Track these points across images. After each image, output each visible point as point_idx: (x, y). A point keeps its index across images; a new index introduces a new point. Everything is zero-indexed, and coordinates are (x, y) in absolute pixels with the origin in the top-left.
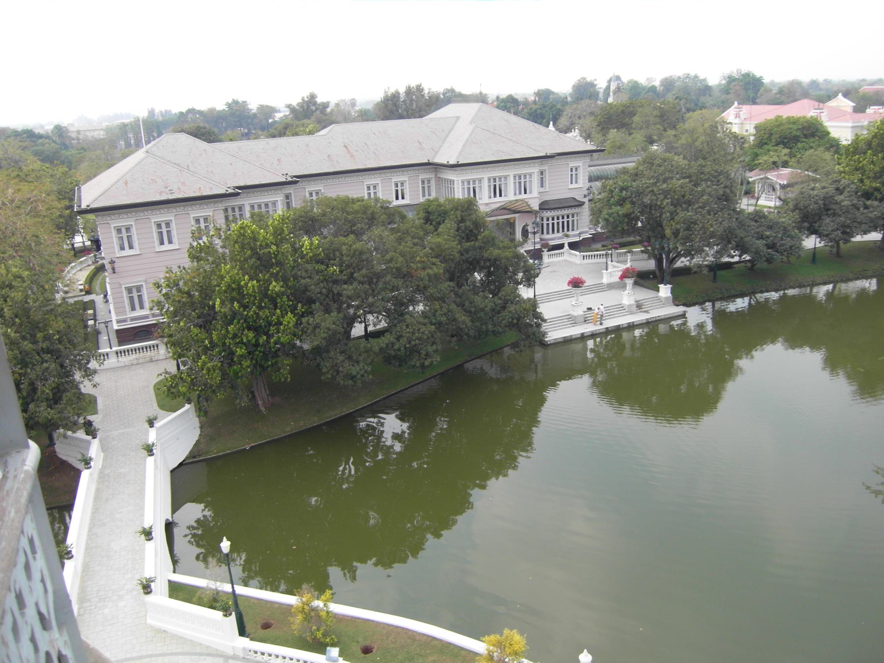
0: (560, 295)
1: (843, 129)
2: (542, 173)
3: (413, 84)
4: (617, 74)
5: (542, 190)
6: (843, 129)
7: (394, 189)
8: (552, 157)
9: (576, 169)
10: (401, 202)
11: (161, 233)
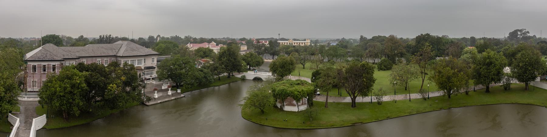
1: (216, 49)
6: (216, 49)
8: (148, 55)
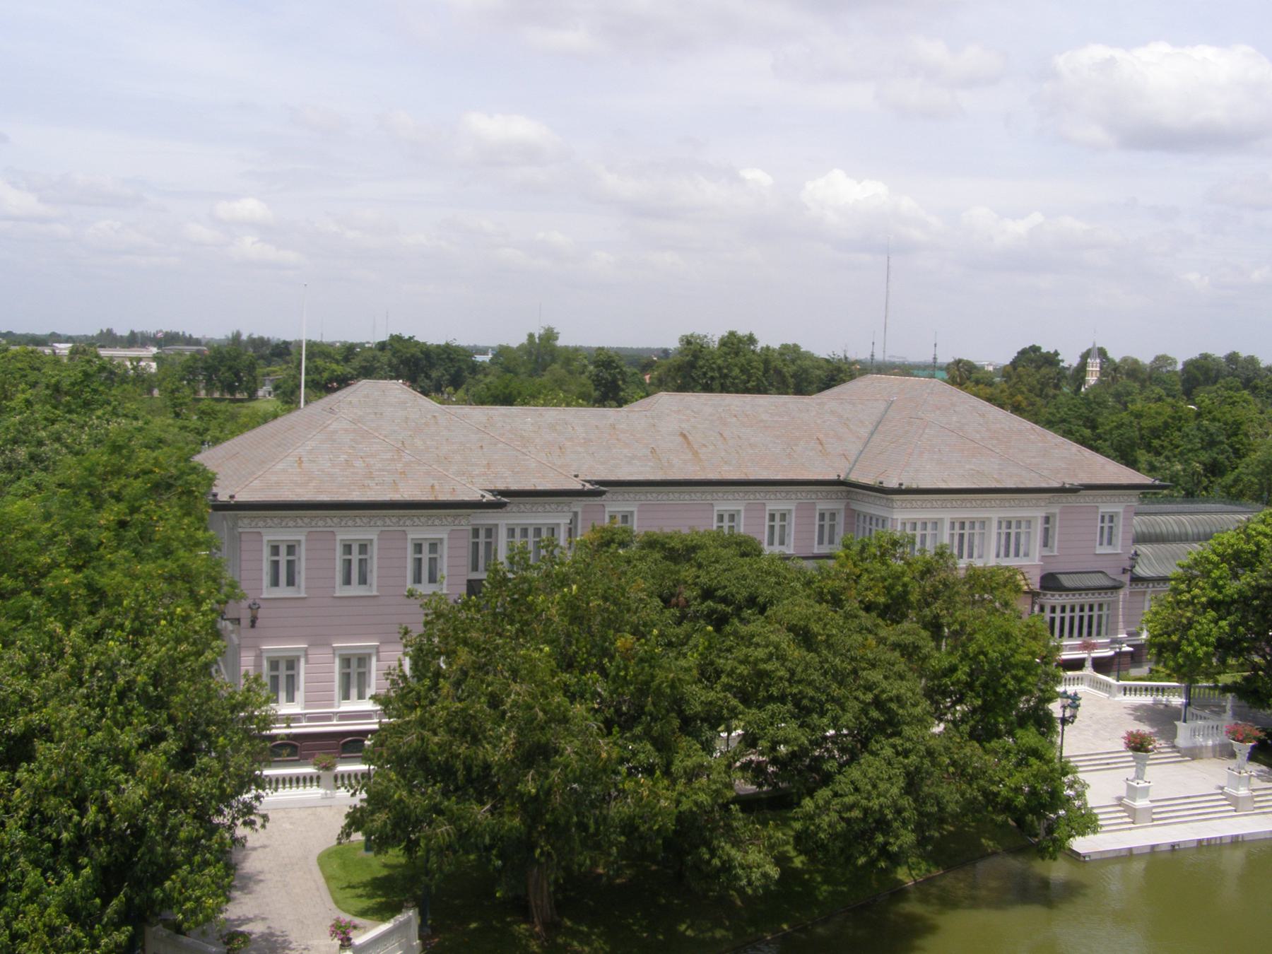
0: (1106, 763)
2: (1047, 520)
3: (742, 331)
7: (767, 523)
8: (1073, 490)
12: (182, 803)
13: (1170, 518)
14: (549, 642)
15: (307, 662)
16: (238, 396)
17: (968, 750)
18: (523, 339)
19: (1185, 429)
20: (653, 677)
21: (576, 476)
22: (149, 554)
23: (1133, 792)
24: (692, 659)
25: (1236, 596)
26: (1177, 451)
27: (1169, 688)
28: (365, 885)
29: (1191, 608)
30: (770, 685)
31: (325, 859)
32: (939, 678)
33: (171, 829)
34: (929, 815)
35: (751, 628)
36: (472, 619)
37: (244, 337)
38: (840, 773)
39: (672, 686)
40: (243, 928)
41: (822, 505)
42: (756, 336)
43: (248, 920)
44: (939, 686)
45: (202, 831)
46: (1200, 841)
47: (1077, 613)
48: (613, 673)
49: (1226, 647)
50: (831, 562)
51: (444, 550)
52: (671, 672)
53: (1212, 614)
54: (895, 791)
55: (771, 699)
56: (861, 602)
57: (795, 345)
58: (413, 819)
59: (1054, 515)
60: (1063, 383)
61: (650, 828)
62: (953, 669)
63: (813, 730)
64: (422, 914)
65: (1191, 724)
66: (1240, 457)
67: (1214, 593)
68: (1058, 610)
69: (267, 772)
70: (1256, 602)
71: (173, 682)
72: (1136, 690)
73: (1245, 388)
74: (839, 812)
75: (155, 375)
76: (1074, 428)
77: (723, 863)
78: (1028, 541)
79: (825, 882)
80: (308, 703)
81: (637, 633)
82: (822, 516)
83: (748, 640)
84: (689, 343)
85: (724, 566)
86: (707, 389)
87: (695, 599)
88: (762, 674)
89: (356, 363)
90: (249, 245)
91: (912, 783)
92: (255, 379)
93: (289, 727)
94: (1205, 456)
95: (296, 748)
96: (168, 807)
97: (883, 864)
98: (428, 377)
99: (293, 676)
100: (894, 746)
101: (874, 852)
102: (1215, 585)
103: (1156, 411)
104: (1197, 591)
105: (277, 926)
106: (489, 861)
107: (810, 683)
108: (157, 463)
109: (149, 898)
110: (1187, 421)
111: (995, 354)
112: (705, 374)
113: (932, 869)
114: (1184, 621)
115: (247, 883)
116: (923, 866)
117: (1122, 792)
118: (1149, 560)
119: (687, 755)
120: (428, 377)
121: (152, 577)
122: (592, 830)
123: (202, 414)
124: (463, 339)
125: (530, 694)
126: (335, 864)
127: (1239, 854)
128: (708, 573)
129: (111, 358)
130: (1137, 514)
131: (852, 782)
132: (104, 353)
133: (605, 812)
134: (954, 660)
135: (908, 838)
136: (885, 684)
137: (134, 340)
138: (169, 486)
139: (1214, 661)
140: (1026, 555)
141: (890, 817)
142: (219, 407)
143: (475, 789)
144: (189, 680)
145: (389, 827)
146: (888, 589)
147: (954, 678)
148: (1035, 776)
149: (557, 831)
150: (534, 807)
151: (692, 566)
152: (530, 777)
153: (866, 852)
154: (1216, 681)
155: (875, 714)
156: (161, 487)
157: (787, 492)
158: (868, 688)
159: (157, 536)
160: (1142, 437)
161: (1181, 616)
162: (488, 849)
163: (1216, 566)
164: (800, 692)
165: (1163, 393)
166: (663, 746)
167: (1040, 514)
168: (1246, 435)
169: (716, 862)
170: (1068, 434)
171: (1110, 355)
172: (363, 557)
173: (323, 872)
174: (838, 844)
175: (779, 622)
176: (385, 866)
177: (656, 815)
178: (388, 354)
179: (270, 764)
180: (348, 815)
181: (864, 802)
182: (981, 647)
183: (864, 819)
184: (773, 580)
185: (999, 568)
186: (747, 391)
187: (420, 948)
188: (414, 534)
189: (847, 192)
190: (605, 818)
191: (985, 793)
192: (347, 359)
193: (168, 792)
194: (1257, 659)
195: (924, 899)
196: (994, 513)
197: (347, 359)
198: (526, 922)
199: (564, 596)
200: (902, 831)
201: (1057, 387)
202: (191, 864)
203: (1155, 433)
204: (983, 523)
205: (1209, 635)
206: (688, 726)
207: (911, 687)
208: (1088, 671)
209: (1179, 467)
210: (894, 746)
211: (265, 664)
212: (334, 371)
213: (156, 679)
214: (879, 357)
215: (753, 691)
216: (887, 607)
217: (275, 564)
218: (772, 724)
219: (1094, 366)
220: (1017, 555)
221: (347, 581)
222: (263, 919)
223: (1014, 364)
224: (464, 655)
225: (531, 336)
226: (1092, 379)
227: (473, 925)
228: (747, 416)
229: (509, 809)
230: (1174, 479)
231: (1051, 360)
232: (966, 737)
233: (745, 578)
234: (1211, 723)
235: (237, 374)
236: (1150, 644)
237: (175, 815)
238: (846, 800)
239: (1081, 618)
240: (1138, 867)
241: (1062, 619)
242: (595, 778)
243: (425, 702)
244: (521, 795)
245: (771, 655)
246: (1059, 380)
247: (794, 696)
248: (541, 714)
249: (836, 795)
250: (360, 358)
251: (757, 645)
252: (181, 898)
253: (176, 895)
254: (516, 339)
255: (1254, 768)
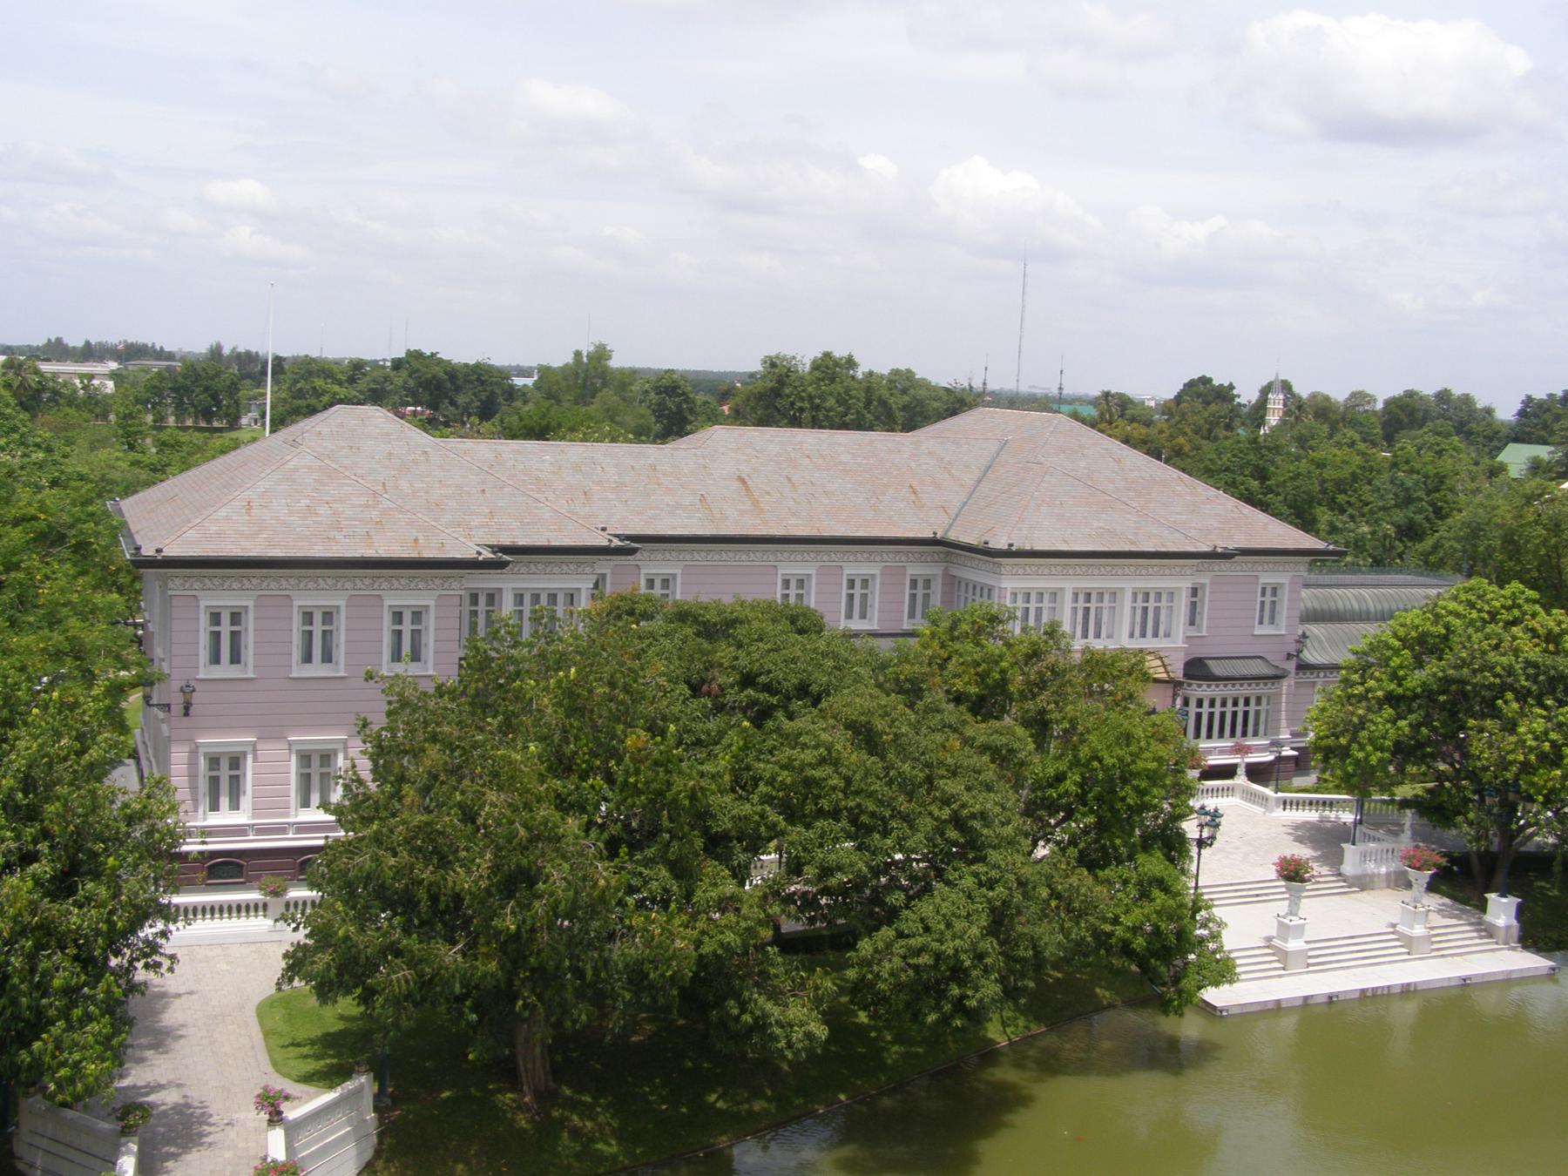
0: (1251, 894)
2: (1194, 592)
3: (840, 352)
4: (1282, 377)
5: (1192, 632)
7: (845, 591)
8: (1227, 555)
9: (1274, 591)
10: (857, 625)
11: (216, 636)
12: (59, 941)
13: (1349, 592)
14: (541, 739)
15: (255, 759)
16: (216, 424)
17: (1074, 880)
18: (569, 359)
19: (1376, 482)
20: (669, 784)
21: (604, 529)
22: (30, 624)
23: (1285, 930)
24: (723, 762)
25: (1419, 690)
26: (1366, 509)
27: (1338, 801)
28: (313, 1043)
29: (1364, 704)
30: (819, 797)
31: (264, 1010)
32: (1041, 788)
33: (43, 975)
34: (1023, 960)
35: (798, 724)
36: (446, 709)
37: (226, 351)
38: (907, 907)
39: (693, 797)
40: (152, 1098)
41: (914, 570)
42: (857, 359)
43: (159, 1087)
44: (1043, 799)
45: (83, 978)
46: (1363, 991)
47: (1229, 708)
48: (621, 779)
49: (1405, 752)
50: (913, 641)
51: (431, 621)
52: (691, 778)
53: (1388, 711)
54: (974, 931)
55: (821, 813)
56: (948, 692)
57: (909, 371)
58: (363, 960)
59: (1203, 586)
60: (1237, 422)
61: (662, 975)
62: (1060, 778)
63: (874, 853)
64: (379, 1078)
65: (1360, 847)
66: (1443, 518)
67: (1393, 686)
68: (1206, 704)
69: (177, 899)
70: (1442, 698)
71: (49, 787)
72: (1298, 804)
73: (1458, 433)
74: (904, 958)
75: (112, 396)
76: (1239, 478)
77: (756, 1019)
78: (1170, 616)
79: (895, 1041)
80: (256, 810)
81: (654, 729)
82: (914, 583)
83: (793, 740)
84: (773, 365)
85: (769, 646)
86: (795, 422)
87: (732, 686)
88: (809, 783)
89: (363, 384)
90: (244, 237)
91: (1000, 921)
92: (237, 403)
93: (204, 843)
94: (1399, 516)
95: (226, 868)
96: (39, 947)
97: (959, 1023)
98: (453, 403)
99: (237, 777)
100: (976, 875)
101: (947, 1007)
102: (1394, 676)
103: (1339, 456)
104: (1372, 683)
105: (195, 1094)
106: (462, 1014)
107: (871, 795)
108: (43, 508)
109: (12, 1063)
110: (1379, 472)
111: (1154, 385)
112: (792, 404)
113: (1032, 1026)
114: (1355, 720)
115: (162, 1039)
116: (1021, 1022)
117: (1272, 931)
118: (1320, 642)
119: (715, 882)
120: (453, 403)
121: (31, 653)
122: (589, 974)
123: (162, 446)
124: (499, 355)
125: (510, 805)
126: (277, 1019)
127: (1411, 1007)
128: (749, 654)
129: (55, 375)
130: (1307, 586)
131: (922, 920)
132: (46, 367)
133: (606, 954)
134: (1062, 766)
135: (991, 988)
136: (966, 797)
137: (89, 353)
138: (61, 539)
139: (1391, 769)
140: (1167, 635)
141: (968, 963)
142: (184, 437)
143: (445, 924)
144: (71, 784)
145: (333, 971)
146: (983, 677)
147: (1061, 789)
148: (1158, 913)
149: (544, 978)
150: (515, 948)
151: (729, 645)
152: (509, 910)
153: (938, 1008)
154: (1393, 794)
155: (953, 834)
156: (50, 539)
157: (871, 553)
158: (946, 802)
159: (41, 601)
160: (1324, 491)
161: (1353, 714)
162: (460, 999)
163: (1397, 652)
164: (859, 806)
165: (1357, 437)
166: (682, 871)
167: (1183, 584)
168: (1451, 490)
169: (747, 1018)
170: (1231, 487)
171: (1296, 389)
172: (326, 628)
173: (261, 1024)
174: (902, 996)
175: (835, 717)
176: (342, 1018)
177: (670, 959)
178: (404, 373)
179: (177, 891)
180: (286, 956)
181: (935, 945)
182: (1094, 750)
183: (935, 967)
184: (830, 663)
185: (1124, 650)
186: (844, 426)
187: (375, 1124)
188: (393, 600)
189: (987, 185)
190: (606, 962)
191: (1096, 933)
192: (352, 380)
193: (39, 927)
194: (1442, 767)
195: (1019, 1064)
196: (1128, 582)
197: (352, 380)
198: (511, 1090)
199: (560, 681)
200: (983, 981)
201: (1229, 427)
202: (68, 1020)
203: (1341, 486)
204: (1114, 594)
205: (1384, 738)
206: (717, 845)
207: (1000, 804)
208: (1241, 780)
209: (1366, 529)
210: (976, 875)
211: (202, 763)
212: (335, 393)
213: (28, 784)
214: (992, 386)
215: (799, 803)
216: (982, 699)
217: (216, 636)
218: (821, 845)
219: (1276, 402)
220: (1156, 635)
221: (308, 658)
222: (179, 1086)
223: (1178, 399)
224: (434, 754)
225: (578, 354)
226: (1273, 419)
227: (446, 1094)
228: (823, 457)
229: (484, 950)
230: (1358, 545)
231: (1224, 394)
232: (1074, 863)
233: (794, 660)
234: (1385, 845)
235: (215, 397)
236: (1317, 748)
237: (49, 957)
238: (912, 941)
239: (1235, 714)
240: (1289, 1023)
241: (1211, 715)
242: (593, 913)
243: (383, 814)
244: (498, 933)
245: (822, 761)
246: (1231, 419)
247: (849, 810)
248: (522, 832)
249: (901, 935)
250: (368, 378)
251: (805, 746)
252: (54, 1063)
253: (47, 1059)
254: (560, 358)
255: (1435, 901)
